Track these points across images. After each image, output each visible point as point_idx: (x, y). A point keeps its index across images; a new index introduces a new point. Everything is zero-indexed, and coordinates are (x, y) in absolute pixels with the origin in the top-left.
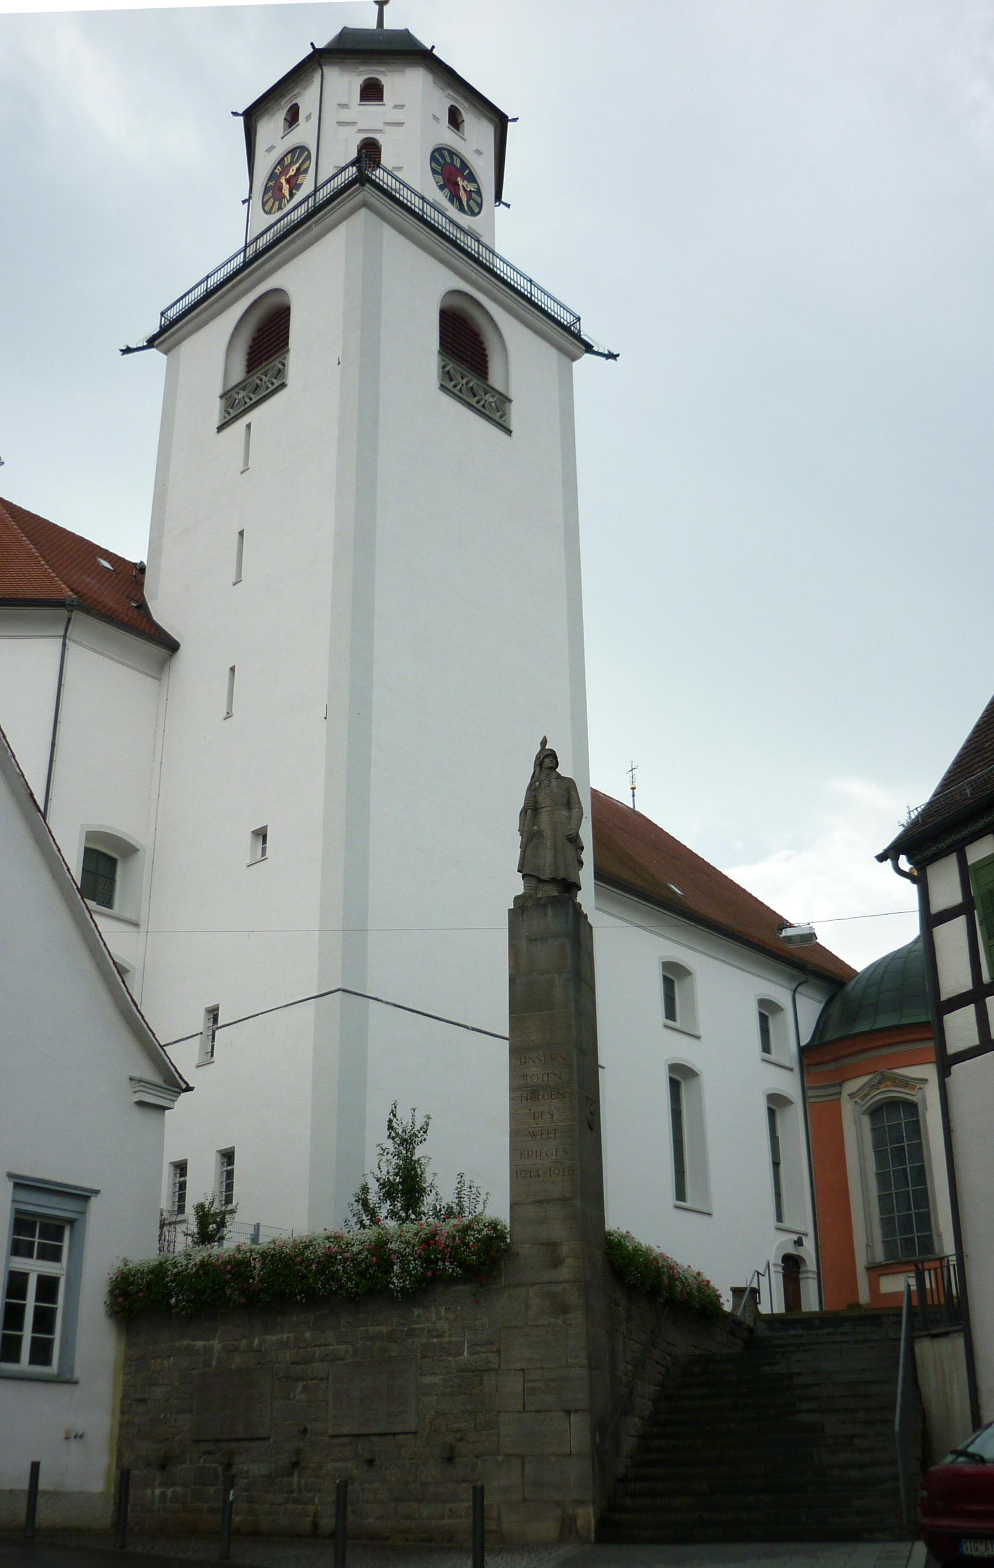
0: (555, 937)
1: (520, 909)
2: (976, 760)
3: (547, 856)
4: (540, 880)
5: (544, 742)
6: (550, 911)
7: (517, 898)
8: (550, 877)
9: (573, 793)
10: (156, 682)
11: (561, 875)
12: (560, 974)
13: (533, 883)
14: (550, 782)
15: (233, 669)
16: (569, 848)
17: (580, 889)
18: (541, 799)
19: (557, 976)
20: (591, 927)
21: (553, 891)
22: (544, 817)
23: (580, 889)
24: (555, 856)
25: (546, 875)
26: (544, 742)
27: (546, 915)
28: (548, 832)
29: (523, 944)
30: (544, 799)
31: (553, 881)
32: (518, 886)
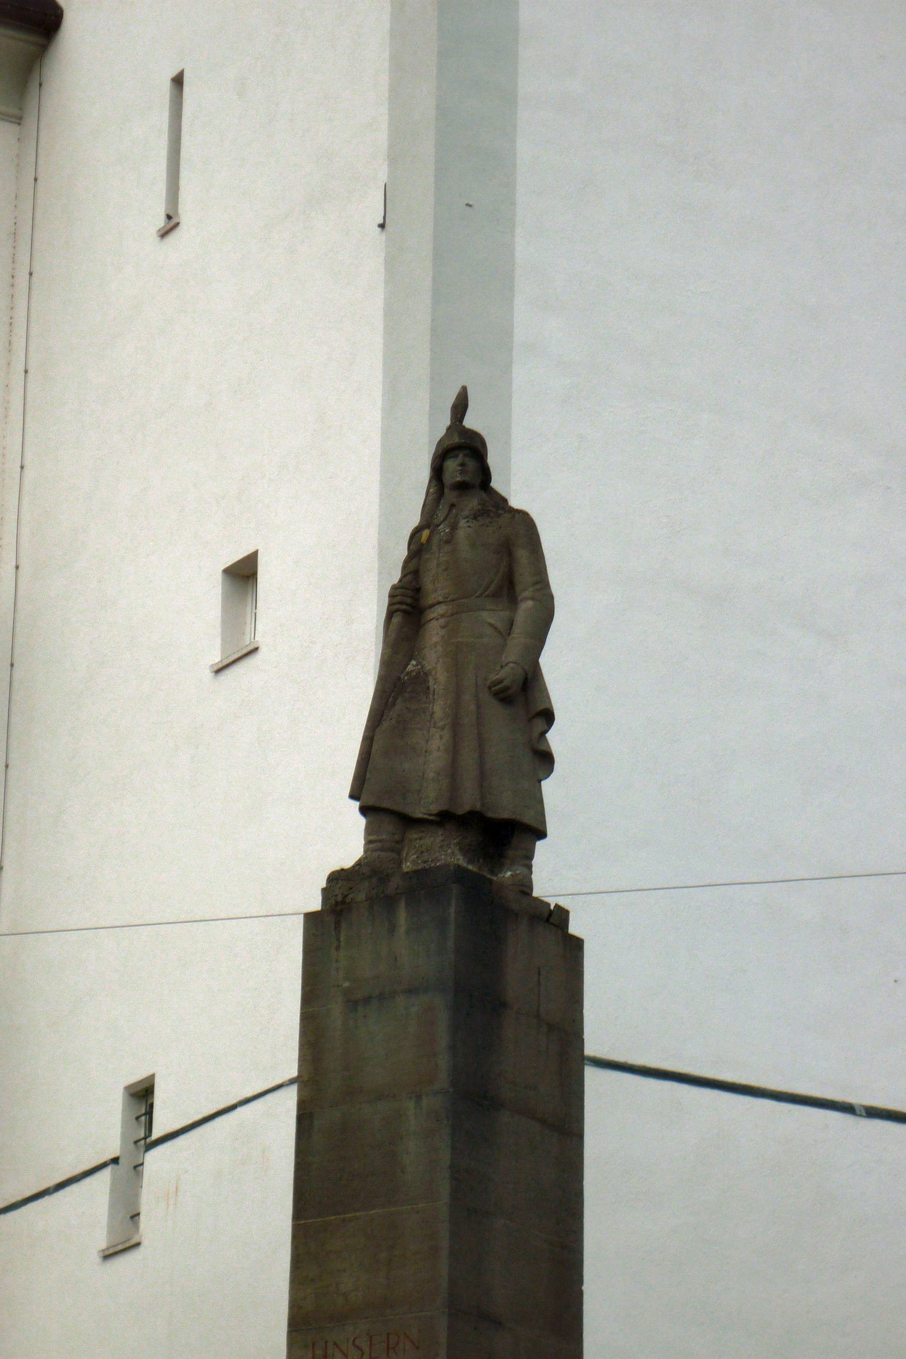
0: (412, 991)
1: (343, 911)
2: (469, 759)
3: (434, 747)
4: (407, 822)
5: (461, 406)
6: (402, 916)
7: (337, 878)
8: (435, 808)
9: (522, 555)
10: (15, 127)
11: (468, 801)
12: (419, 1098)
13: (389, 827)
14: (454, 527)
15: (178, 81)
16: (500, 724)
17: (541, 834)
18: (428, 583)
19: (411, 1105)
20: (577, 945)
21: (446, 852)
22: (434, 632)
23: (542, 835)
24: (454, 750)
25: (427, 804)
26: (461, 406)
27: (392, 928)
28: (440, 678)
29: (336, 1010)
30: (436, 587)
31: (445, 818)
32: (345, 839)
